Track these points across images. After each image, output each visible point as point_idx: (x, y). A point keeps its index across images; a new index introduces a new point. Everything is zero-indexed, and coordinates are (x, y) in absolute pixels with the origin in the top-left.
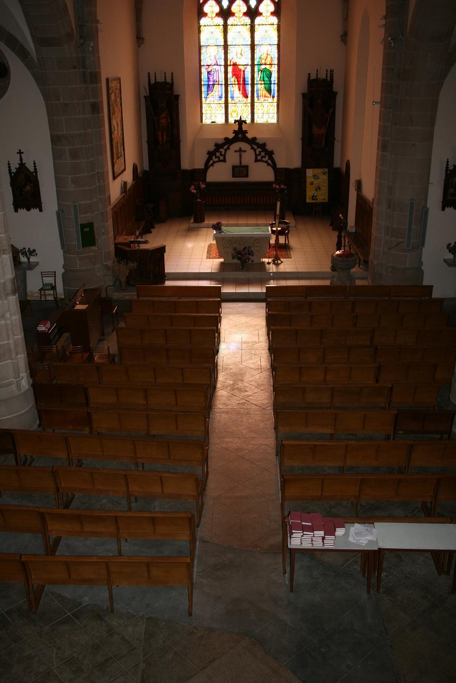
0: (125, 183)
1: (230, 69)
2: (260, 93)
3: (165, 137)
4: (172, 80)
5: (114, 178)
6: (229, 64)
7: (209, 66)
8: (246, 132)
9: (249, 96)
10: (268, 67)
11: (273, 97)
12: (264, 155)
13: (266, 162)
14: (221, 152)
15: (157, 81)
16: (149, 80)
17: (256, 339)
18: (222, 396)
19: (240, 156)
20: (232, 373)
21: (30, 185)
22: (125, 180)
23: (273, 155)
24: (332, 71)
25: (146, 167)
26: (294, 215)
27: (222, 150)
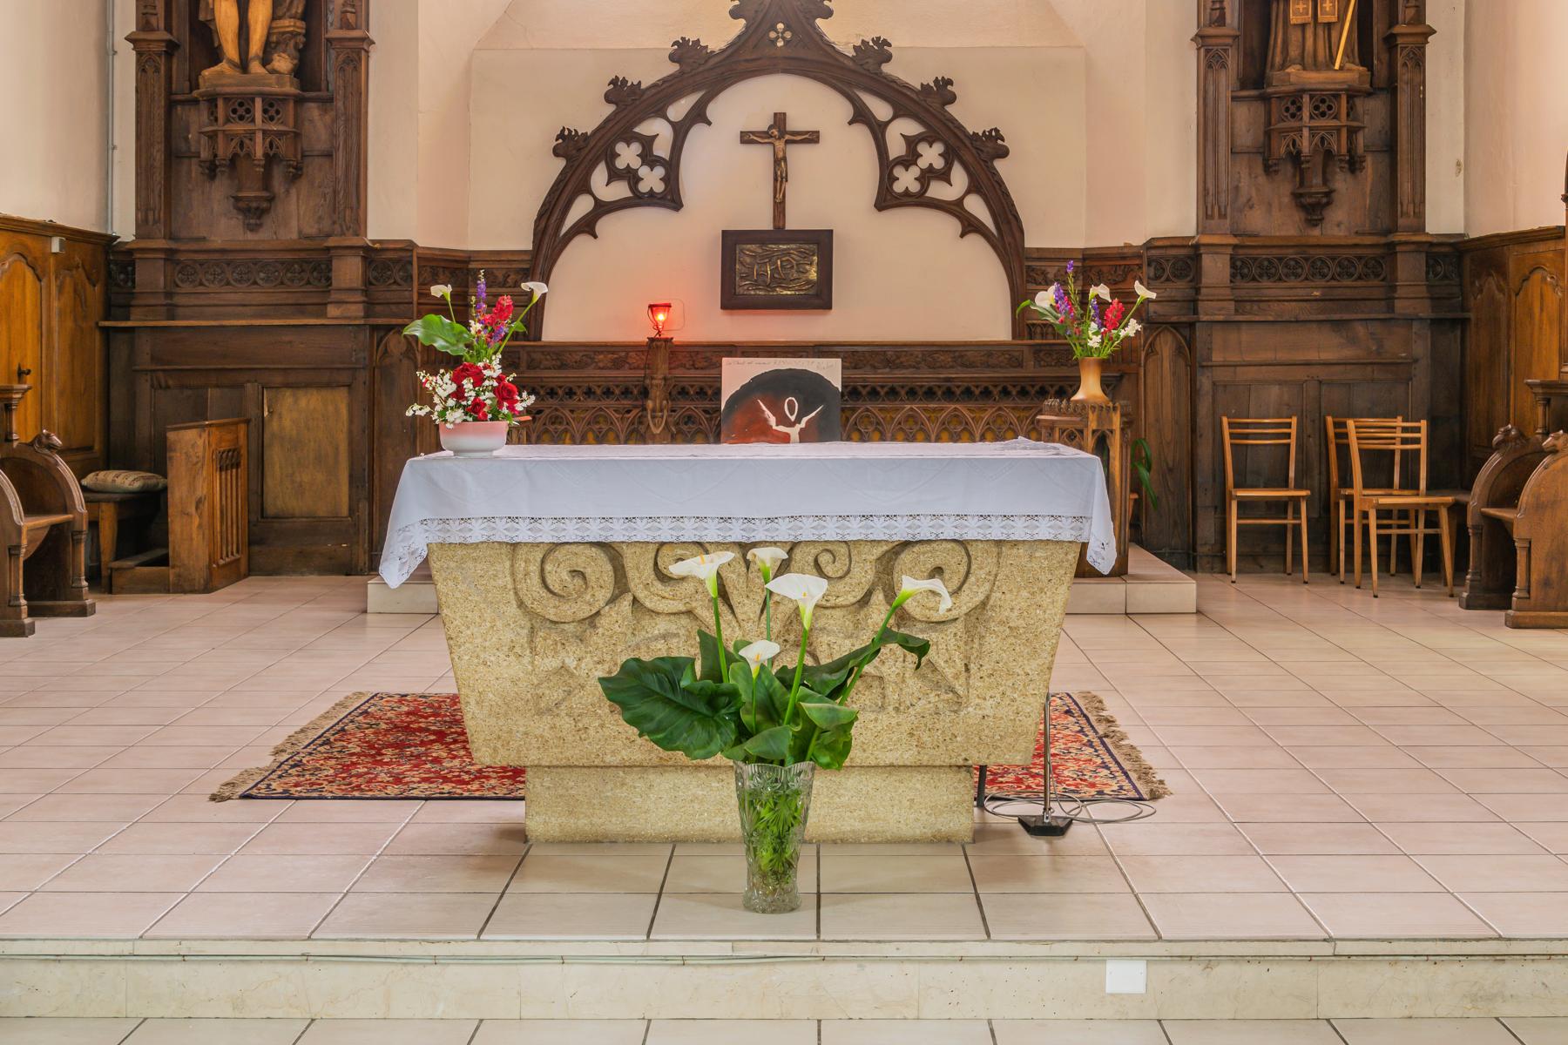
13: (954, 208)
14: (647, 142)
19: (779, 162)
23: (999, 165)
27: (658, 129)
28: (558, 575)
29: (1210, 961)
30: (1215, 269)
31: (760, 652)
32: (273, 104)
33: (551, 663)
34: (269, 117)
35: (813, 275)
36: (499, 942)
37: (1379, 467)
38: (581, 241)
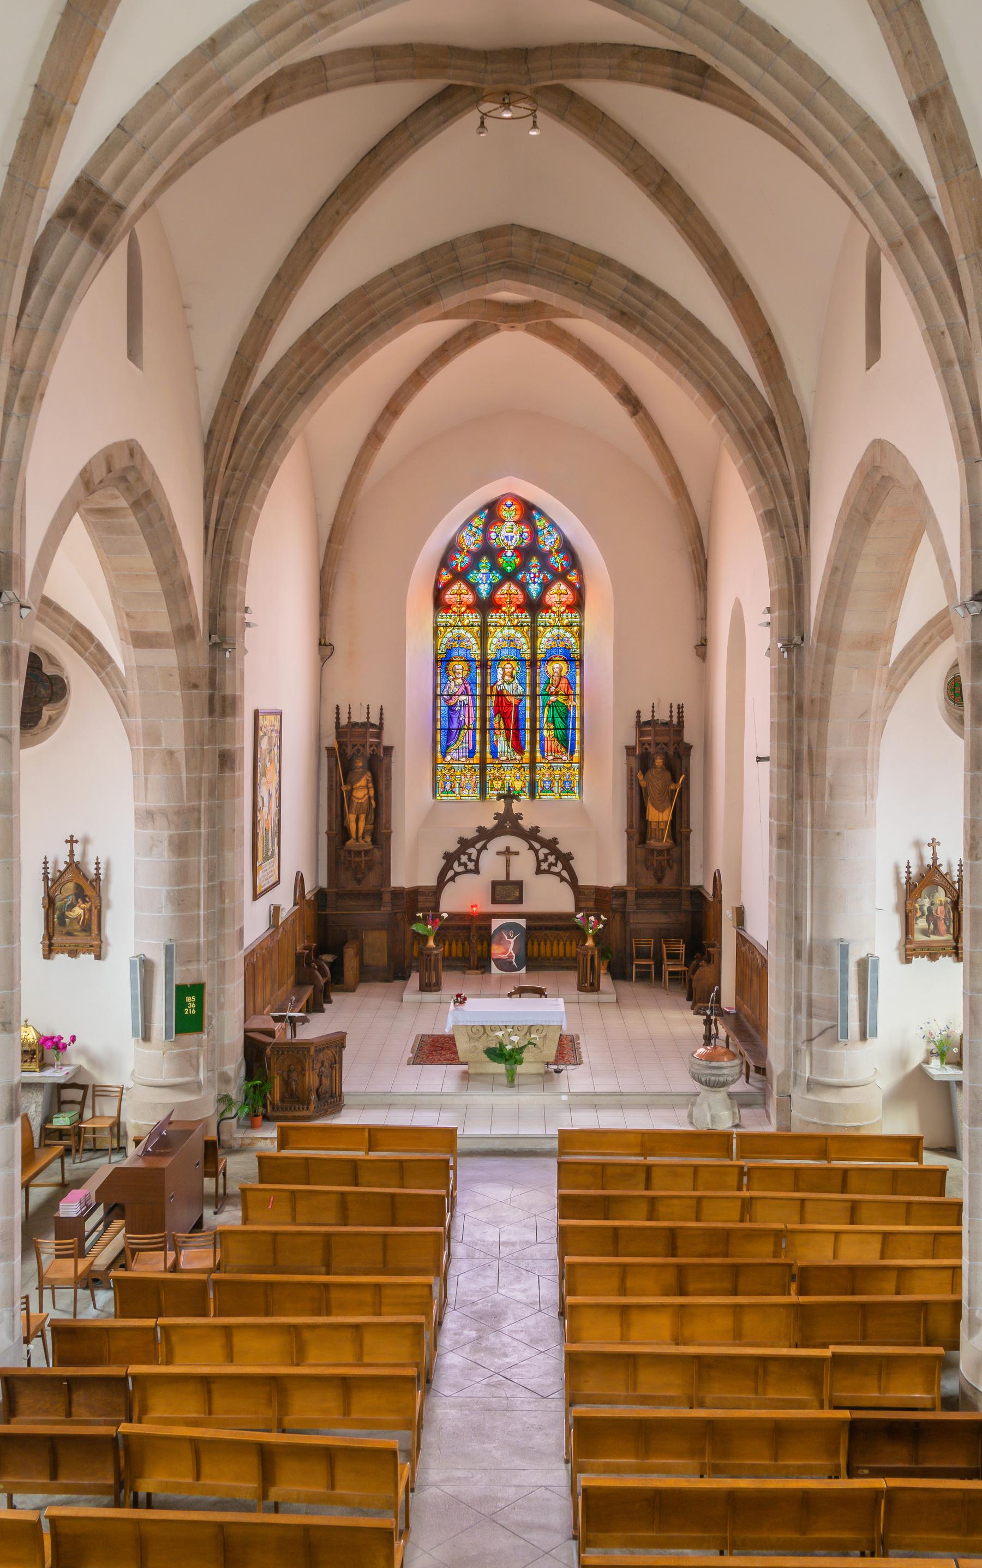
0: (277, 909)
1: (491, 702)
2: (547, 745)
3: (362, 825)
4: (381, 719)
5: (256, 897)
6: (489, 693)
7: (451, 696)
8: (519, 816)
9: (527, 747)
10: (561, 699)
11: (572, 753)
12: (554, 861)
13: (558, 874)
14: (470, 855)
15: (352, 720)
16: (338, 718)
17: (531, 1237)
18: (453, 1366)
19: (508, 862)
20: (475, 1312)
21: (83, 906)
22: (276, 903)
23: (571, 862)
24: (680, 707)
25: (324, 883)
26: (613, 979)
27: (472, 851)
28: (474, 1030)
29: (577, 1095)
30: (631, 897)
31: (509, 1047)
32: (366, 852)
33: (473, 1045)
34: (365, 856)
35: (517, 894)
36: (469, 1093)
37: (673, 956)
38: (451, 883)
